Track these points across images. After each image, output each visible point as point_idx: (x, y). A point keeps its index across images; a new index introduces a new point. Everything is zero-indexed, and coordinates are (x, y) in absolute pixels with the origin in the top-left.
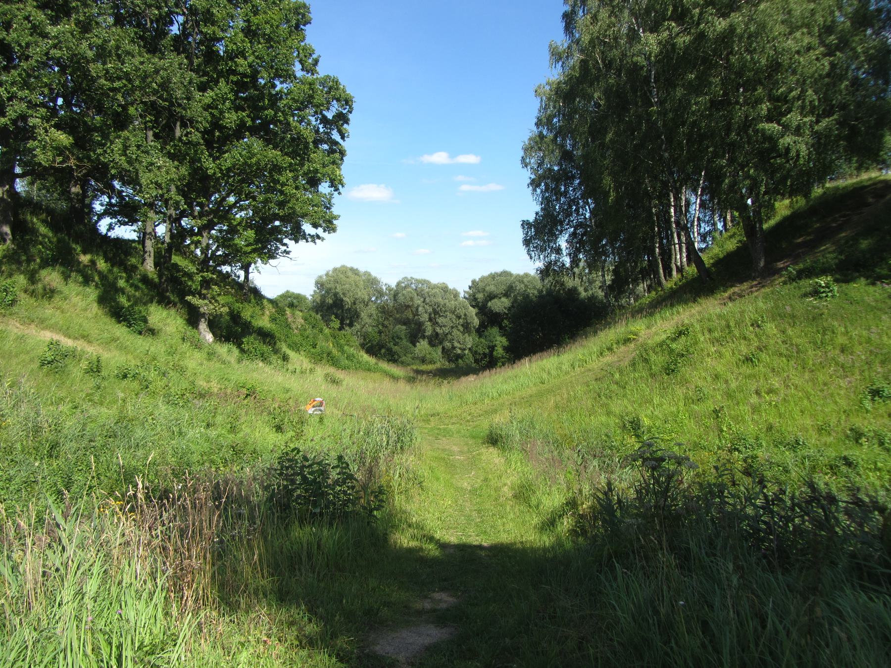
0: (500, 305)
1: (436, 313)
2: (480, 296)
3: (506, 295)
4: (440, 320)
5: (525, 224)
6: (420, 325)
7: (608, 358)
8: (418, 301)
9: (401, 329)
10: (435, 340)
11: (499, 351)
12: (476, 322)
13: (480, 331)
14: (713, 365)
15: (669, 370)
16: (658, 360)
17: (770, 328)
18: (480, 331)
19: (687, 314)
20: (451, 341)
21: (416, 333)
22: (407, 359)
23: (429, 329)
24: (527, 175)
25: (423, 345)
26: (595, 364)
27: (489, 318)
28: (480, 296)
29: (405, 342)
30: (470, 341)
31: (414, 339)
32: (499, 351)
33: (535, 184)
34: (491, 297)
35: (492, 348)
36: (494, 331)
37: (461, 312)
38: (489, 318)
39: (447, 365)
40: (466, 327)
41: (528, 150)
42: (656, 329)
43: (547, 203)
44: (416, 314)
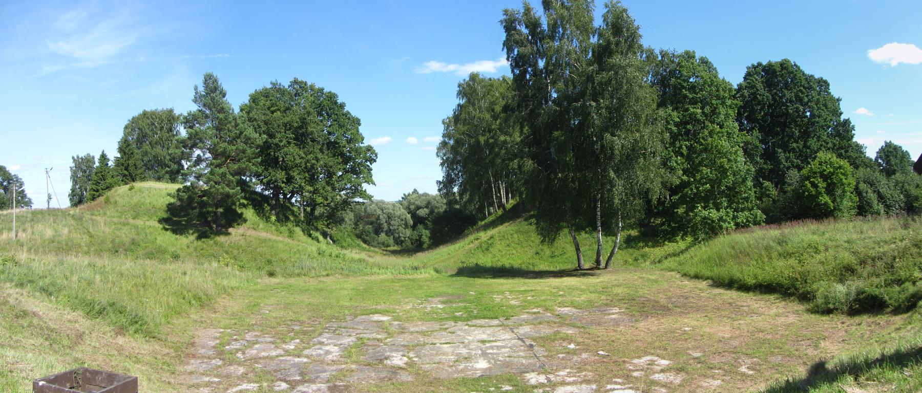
0: (423, 212)
1: (390, 217)
2: (412, 207)
3: (427, 207)
4: (392, 222)
5: (439, 182)
6: (380, 224)
7: (472, 245)
8: (379, 212)
9: (369, 228)
10: (389, 233)
11: (425, 239)
12: (412, 223)
13: (414, 227)
14: (499, 246)
15: (487, 249)
16: (485, 246)
17: (515, 236)
18: (414, 227)
19: (490, 232)
20: (398, 233)
21: (378, 230)
22: (375, 243)
23: (385, 226)
24: (439, 161)
25: (383, 236)
26: (467, 247)
27: (418, 220)
28: (412, 207)
29: (372, 235)
30: (408, 232)
31: (378, 231)
32: (425, 239)
33: (442, 164)
34: (419, 208)
35: (420, 236)
36: (420, 226)
37: (403, 217)
38: (418, 220)
39: (396, 248)
40: (406, 226)
41: (439, 149)
42: (484, 236)
43: (448, 175)
44: (378, 219)
